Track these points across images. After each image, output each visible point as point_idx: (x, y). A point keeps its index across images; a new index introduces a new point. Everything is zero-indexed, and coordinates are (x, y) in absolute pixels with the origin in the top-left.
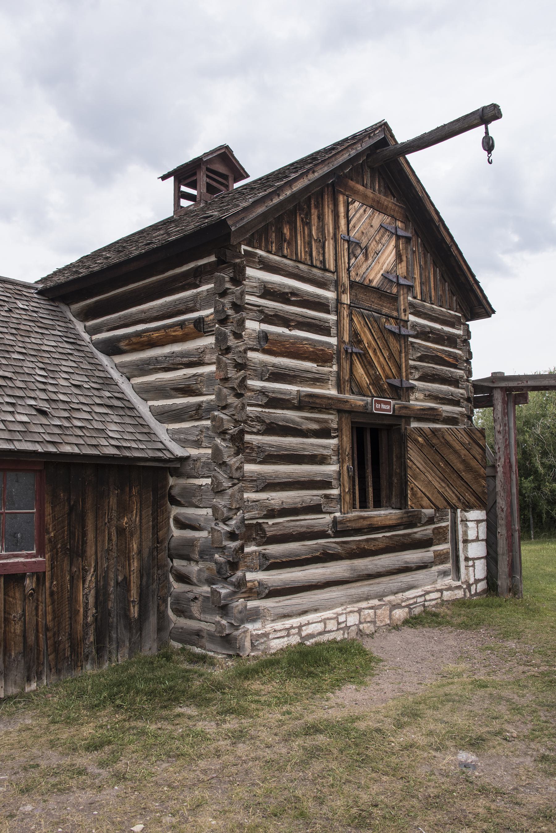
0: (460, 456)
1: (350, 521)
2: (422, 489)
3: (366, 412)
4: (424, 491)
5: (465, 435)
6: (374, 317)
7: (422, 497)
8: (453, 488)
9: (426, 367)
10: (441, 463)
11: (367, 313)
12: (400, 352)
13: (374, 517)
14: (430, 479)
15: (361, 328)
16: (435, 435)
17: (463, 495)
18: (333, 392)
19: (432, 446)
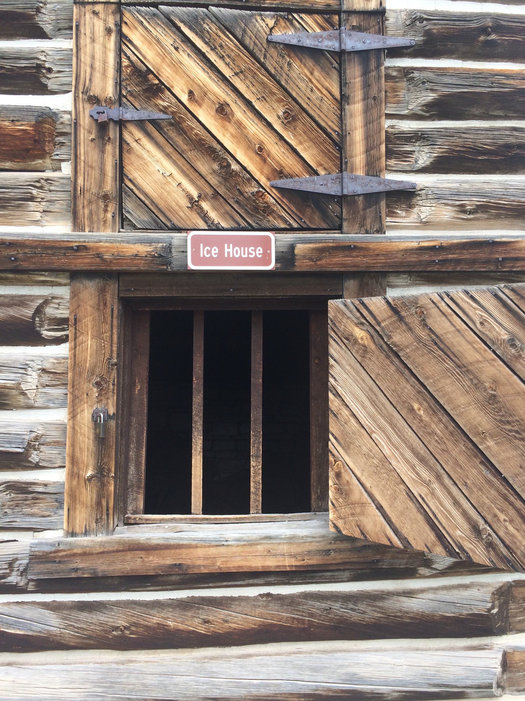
0: (477, 384)
1: (85, 554)
2: (363, 479)
3: (163, 270)
4: (368, 485)
5: (495, 313)
6: (218, 20)
7: (363, 504)
8: (454, 490)
9: (487, 130)
10: (416, 406)
11: (188, 14)
12: (343, 100)
13: (196, 547)
14: (387, 451)
15: (164, 54)
16: (401, 319)
17: (489, 518)
18: (58, 229)
19: (393, 353)
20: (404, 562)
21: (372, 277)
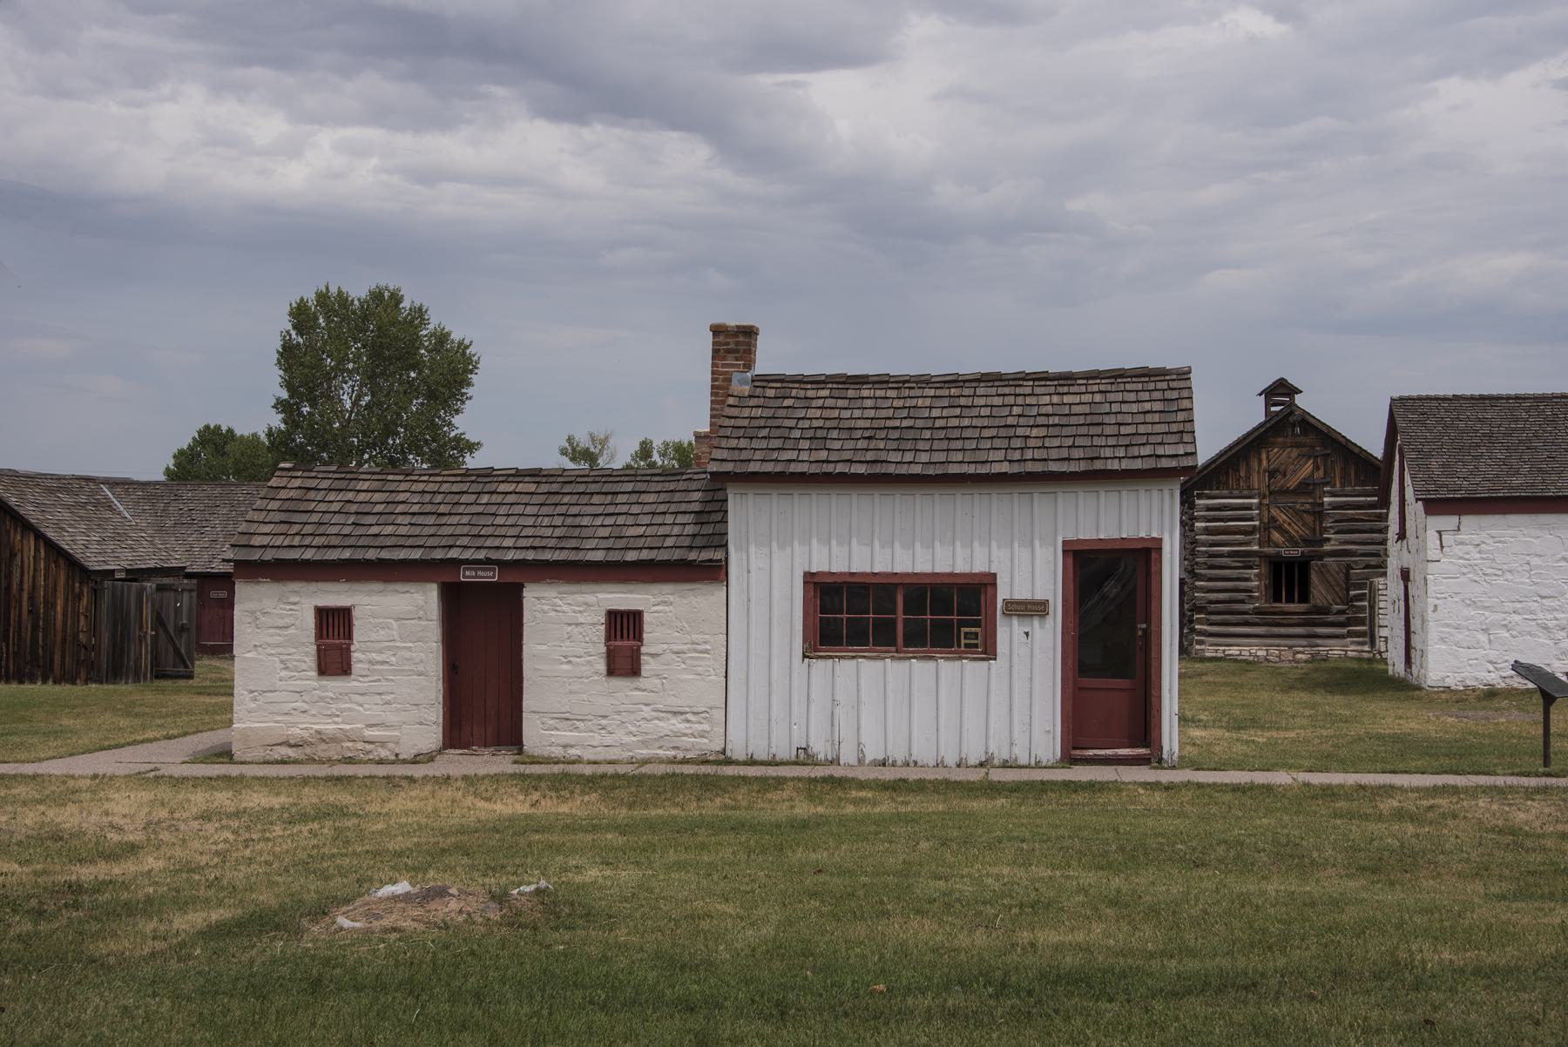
18: (1256, 548)
20: (1326, 611)
21: (1321, 556)
